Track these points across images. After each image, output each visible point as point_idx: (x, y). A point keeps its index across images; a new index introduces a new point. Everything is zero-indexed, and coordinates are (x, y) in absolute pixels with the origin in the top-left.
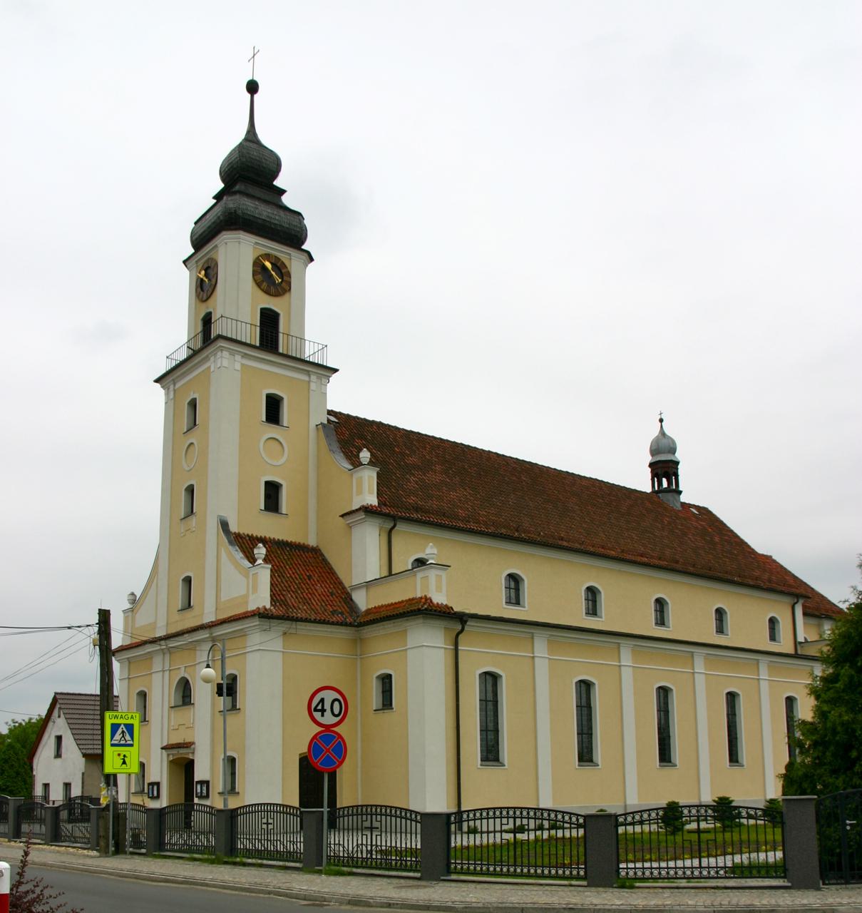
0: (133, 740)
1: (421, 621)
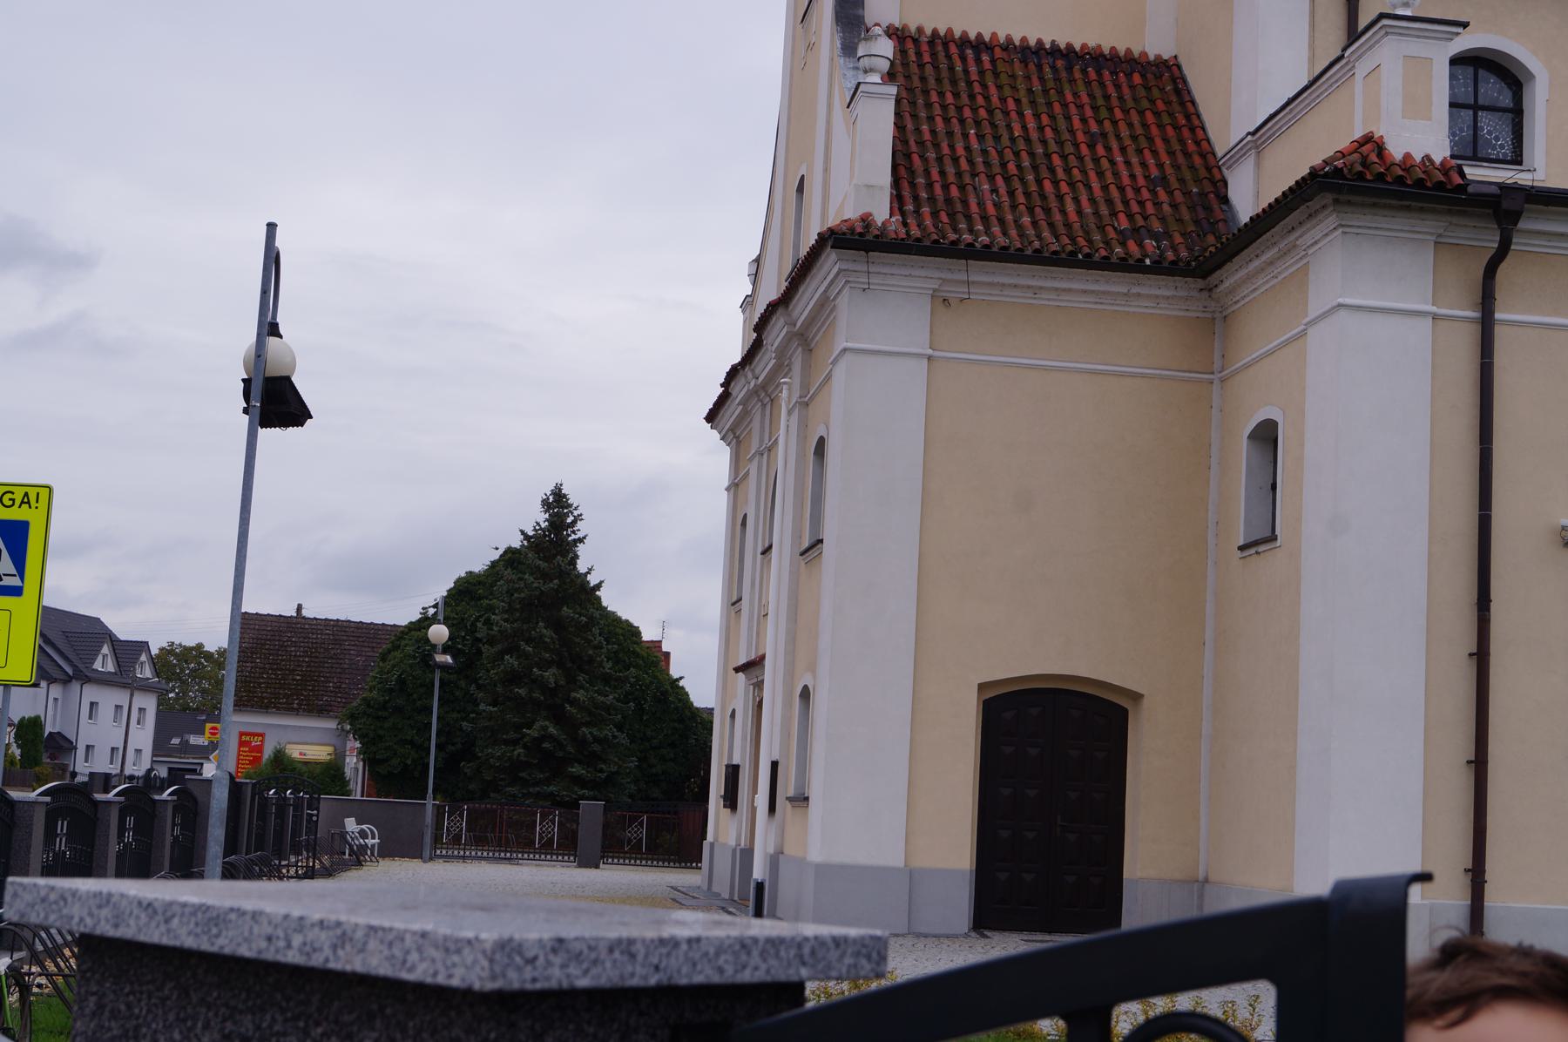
1: (1331, 220)
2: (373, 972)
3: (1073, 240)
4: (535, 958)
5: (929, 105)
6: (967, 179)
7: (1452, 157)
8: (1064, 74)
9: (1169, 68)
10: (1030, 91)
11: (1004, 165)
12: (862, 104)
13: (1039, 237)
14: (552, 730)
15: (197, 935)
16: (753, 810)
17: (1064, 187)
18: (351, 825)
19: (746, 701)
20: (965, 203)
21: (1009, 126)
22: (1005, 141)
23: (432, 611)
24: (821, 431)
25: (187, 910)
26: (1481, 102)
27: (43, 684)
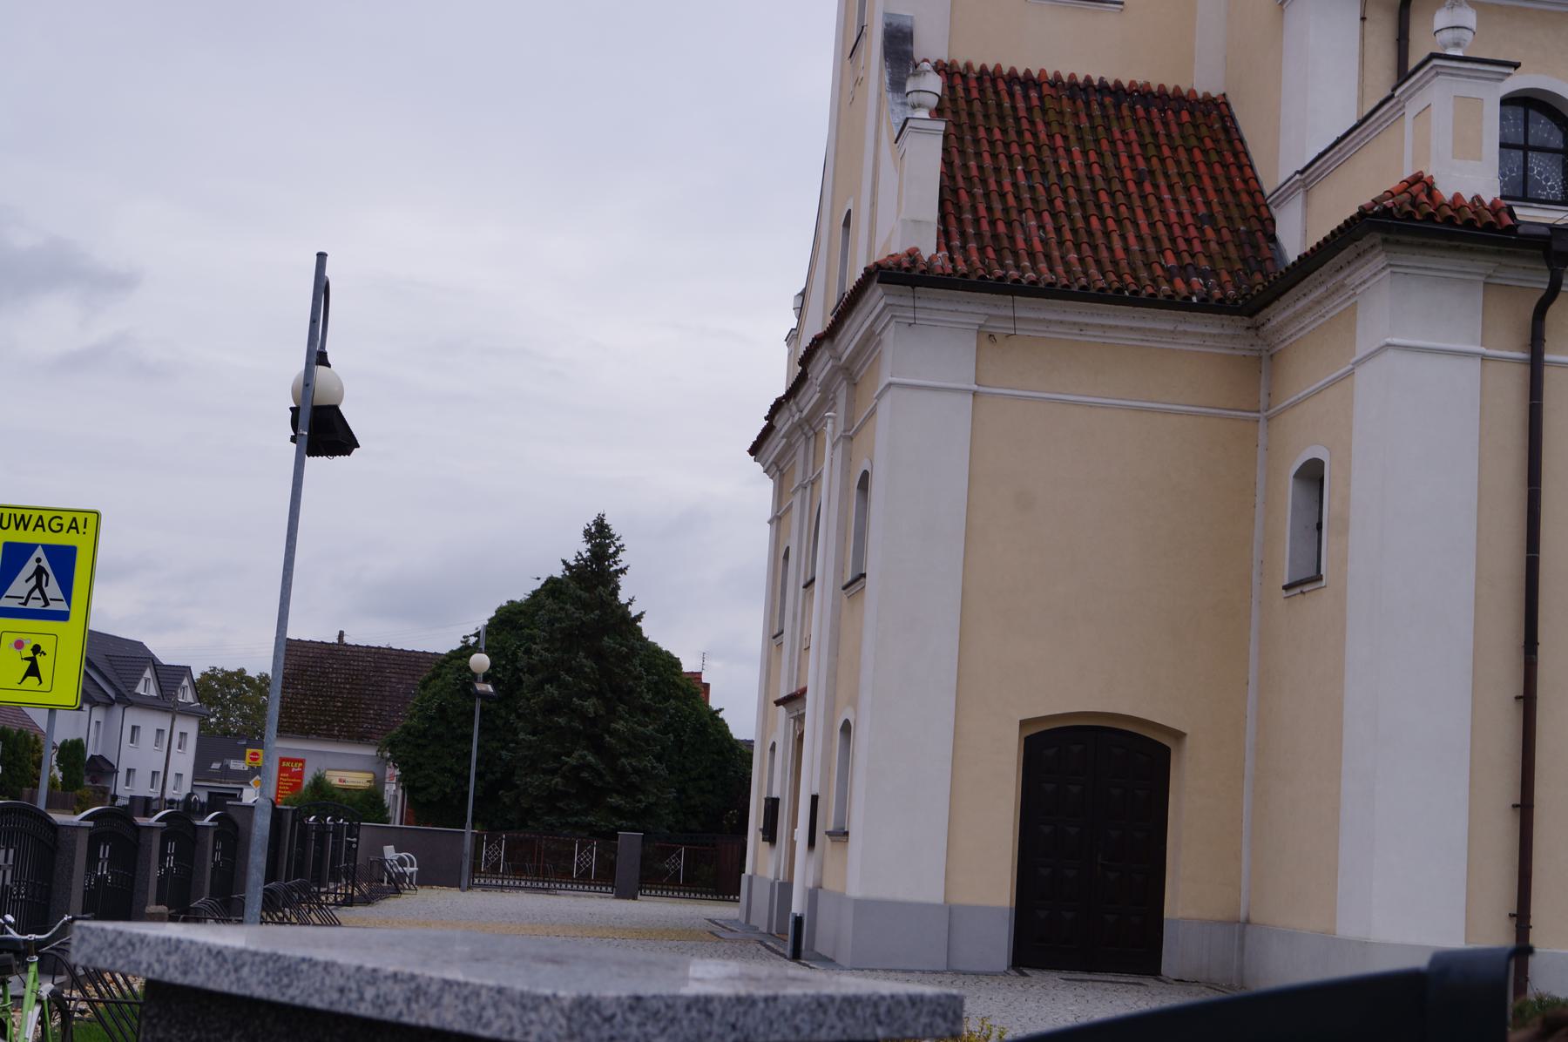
0: (68, 600)
1: (1380, 260)
2: (448, 1027)
3: (1120, 277)
4: (613, 1016)
5: (976, 141)
6: (1014, 215)
7: (1502, 197)
8: (1112, 111)
9: (1217, 106)
10: (1078, 128)
11: (1051, 201)
12: (909, 140)
13: (1086, 273)
14: (591, 758)
15: (268, 985)
16: (793, 844)
17: (1111, 225)
18: (390, 852)
19: (786, 736)
20: (1012, 238)
21: (1056, 163)
22: (1053, 177)
23: (473, 640)
24: (865, 466)
25: (258, 959)
26: (1531, 142)
27: (86, 707)
